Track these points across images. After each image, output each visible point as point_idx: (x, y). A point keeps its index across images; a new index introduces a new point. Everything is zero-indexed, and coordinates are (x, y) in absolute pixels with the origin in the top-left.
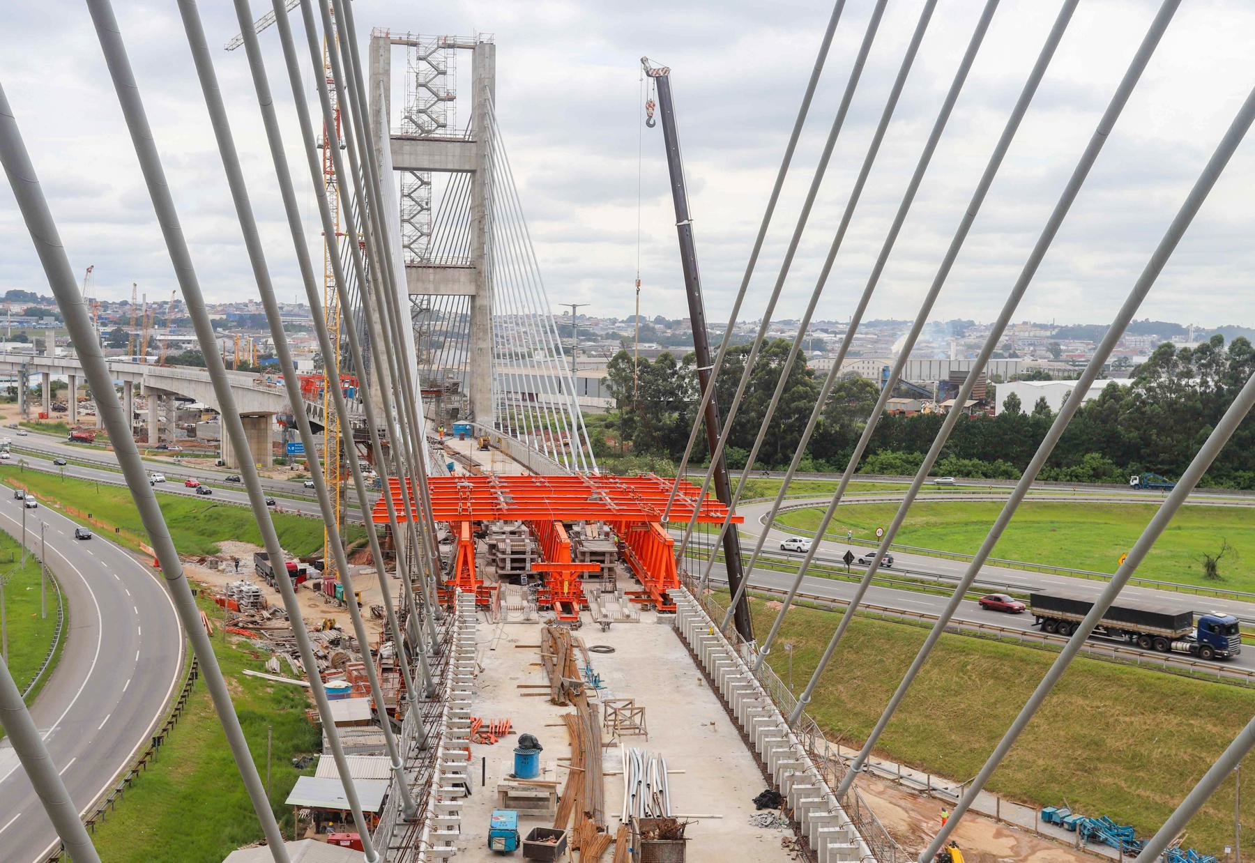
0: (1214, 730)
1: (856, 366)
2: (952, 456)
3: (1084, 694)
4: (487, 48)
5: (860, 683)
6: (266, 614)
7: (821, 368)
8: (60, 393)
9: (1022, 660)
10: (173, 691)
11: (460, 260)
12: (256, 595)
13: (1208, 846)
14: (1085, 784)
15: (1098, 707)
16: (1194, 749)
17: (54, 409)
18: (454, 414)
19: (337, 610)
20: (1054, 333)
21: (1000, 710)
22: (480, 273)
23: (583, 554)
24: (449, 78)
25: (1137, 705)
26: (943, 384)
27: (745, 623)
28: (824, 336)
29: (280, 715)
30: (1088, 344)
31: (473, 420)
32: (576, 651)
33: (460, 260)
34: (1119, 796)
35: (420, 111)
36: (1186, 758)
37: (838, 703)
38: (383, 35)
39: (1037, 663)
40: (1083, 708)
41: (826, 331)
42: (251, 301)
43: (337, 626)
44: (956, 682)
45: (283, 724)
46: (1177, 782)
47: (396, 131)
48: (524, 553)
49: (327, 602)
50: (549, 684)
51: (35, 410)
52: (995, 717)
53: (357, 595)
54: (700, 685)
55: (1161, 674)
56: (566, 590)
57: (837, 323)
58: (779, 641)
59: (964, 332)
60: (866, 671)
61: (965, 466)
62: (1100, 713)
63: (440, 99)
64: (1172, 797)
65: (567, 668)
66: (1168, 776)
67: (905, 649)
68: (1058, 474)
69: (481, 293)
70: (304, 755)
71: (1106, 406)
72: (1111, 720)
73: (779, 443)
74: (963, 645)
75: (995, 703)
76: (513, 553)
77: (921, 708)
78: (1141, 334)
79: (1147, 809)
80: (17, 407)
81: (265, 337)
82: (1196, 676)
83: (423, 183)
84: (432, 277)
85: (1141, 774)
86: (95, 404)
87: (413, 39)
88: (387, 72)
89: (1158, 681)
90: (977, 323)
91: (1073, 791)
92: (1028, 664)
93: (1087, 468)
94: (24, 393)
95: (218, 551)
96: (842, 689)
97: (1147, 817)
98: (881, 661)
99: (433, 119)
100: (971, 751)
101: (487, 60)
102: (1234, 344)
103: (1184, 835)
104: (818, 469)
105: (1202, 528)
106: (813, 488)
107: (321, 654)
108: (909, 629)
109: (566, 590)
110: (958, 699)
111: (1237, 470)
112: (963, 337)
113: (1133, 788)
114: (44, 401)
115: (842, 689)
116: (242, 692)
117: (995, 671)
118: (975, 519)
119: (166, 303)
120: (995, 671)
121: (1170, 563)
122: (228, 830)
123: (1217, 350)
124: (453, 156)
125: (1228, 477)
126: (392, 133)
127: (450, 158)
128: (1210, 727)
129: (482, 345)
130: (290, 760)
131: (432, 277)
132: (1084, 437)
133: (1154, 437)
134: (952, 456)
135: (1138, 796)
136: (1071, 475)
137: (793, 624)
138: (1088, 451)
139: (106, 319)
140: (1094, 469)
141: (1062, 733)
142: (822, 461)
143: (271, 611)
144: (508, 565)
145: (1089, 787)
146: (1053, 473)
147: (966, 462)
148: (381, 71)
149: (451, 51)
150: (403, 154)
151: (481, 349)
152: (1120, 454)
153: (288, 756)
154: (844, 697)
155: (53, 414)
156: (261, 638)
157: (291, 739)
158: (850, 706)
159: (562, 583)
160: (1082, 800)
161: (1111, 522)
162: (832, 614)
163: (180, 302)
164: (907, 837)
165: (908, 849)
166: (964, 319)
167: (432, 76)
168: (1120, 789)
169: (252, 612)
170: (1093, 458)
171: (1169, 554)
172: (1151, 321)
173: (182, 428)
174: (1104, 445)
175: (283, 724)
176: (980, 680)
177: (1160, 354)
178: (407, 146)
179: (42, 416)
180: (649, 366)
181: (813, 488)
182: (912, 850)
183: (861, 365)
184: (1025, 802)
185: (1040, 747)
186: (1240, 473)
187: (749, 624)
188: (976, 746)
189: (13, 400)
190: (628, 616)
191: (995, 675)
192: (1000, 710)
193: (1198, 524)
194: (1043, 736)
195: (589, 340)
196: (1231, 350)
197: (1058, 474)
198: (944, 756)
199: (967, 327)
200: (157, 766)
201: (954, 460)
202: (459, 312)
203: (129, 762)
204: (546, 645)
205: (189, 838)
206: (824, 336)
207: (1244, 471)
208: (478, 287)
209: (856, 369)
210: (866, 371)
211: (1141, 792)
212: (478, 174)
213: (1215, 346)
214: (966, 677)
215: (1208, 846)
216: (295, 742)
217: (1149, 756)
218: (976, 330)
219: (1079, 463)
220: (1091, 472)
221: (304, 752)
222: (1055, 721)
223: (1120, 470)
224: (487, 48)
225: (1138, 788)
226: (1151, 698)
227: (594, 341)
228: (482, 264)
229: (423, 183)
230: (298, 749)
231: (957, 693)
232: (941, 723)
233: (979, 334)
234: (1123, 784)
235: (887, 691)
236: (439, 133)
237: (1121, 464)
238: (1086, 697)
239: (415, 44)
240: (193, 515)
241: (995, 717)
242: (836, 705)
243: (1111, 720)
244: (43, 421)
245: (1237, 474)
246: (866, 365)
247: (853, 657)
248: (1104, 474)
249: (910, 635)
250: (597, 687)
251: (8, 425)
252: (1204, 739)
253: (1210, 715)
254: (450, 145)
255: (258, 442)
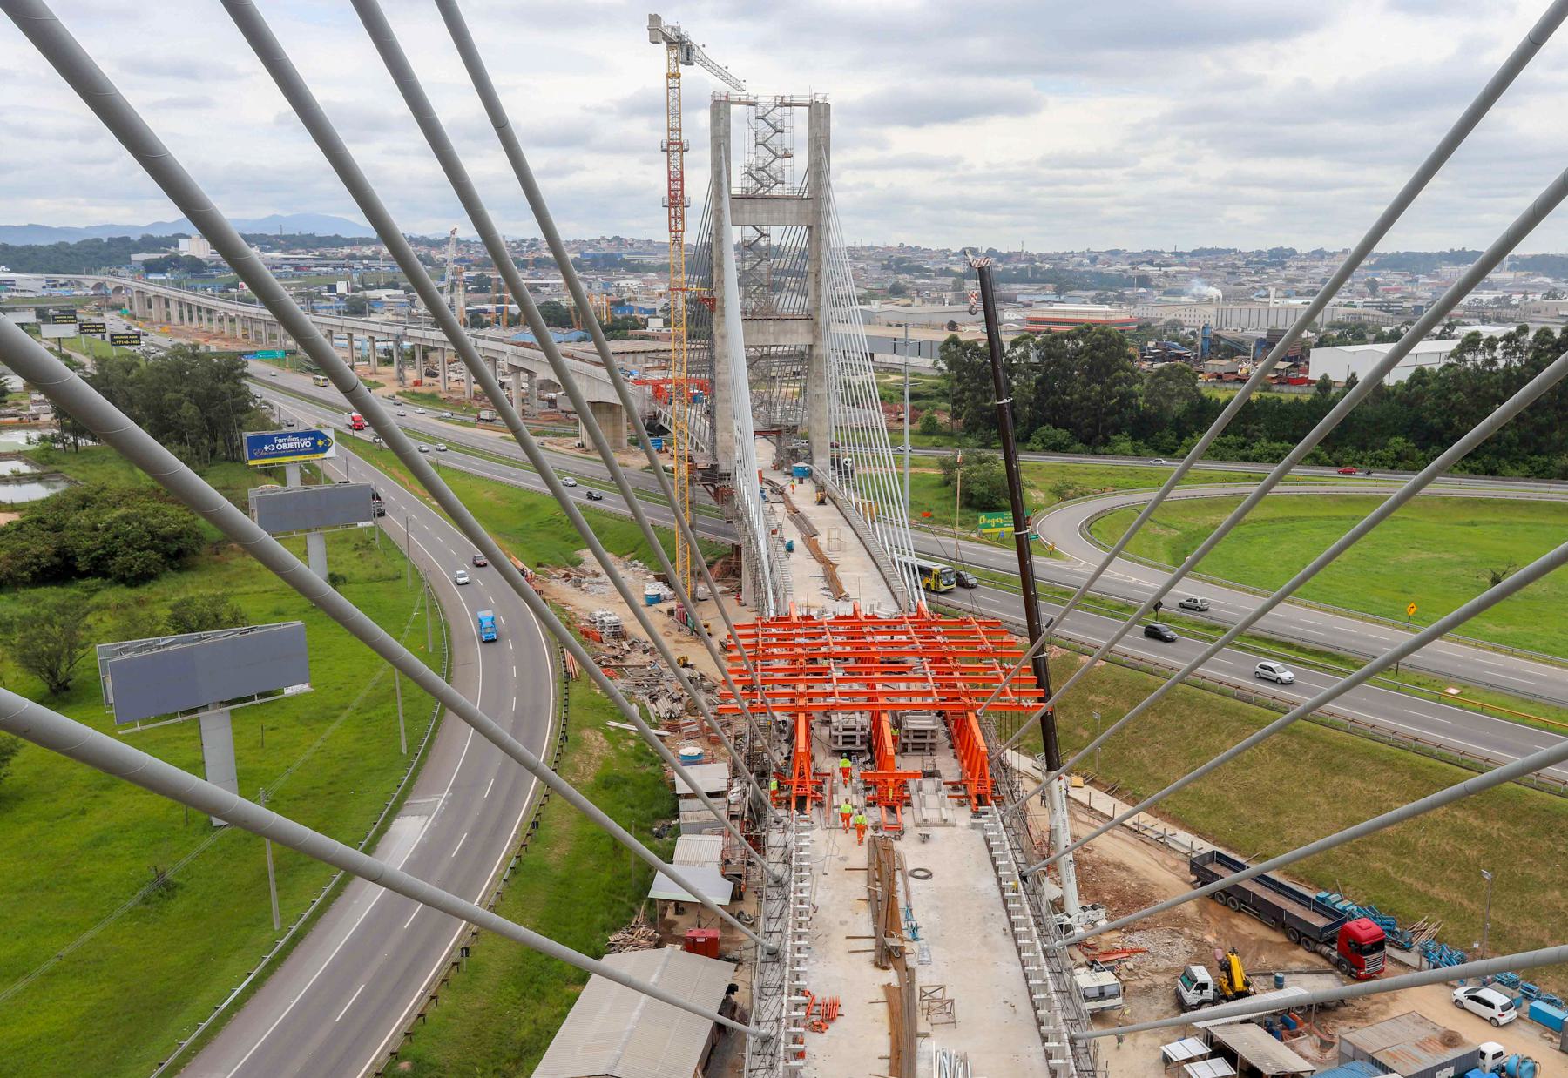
0: (1475, 823)
1: (1178, 313)
2: (1263, 439)
3: (1362, 778)
4: (822, 108)
5: (1161, 747)
6: (625, 645)
7: (1145, 316)
8: (432, 355)
9: (1308, 738)
10: (546, 752)
11: (798, 266)
12: (616, 625)
13: (1459, 937)
14: (1356, 867)
15: (1374, 792)
16: (1456, 841)
17: (427, 374)
18: (794, 454)
19: (688, 639)
20: (1372, 263)
21: (1285, 787)
22: (817, 324)
23: (908, 731)
24: (786, 135)
25: (1409, 792)
26: (1260, 342)
27: (1054, 755)
28: (1150, 270)
29: (641, 775)
30: (1405, 275)
31: (811, 463)
32: (898, 873)
33: (798, 266)
34: (1386, 882)
35: (758, 169)
36: (1448, 848)
37: (1141, 766)
38: (724, 99)
39: (1323, 742)
40: (1360, 791)
41: (1150, 263)
42: (603, 238)
43: (689, 663)
44: (1248, 755)
45: (644, 788)
46: (1438, 872)
47: (736, 191)
48: (854, 729)
49: (680, 630)
50: (873, 935)
51: (411, 374)
52: (1282, 793)
53: (706, 626)
54: (1006, 934)
55: (1432, 762)
56: (890, 796)
57: (1162, 252)
58: (1090, 698)
59: (1285, 263)
60: (1167, 736)
61: (1276, 449)
62: (1375, 797)
63: (777, 157)
64: (1433, 886)
65: (889, 912)
66: (1431, 865)
67: (1204, 717)
68: (1363, 457)
69: (818, 343)
70: (663, 822)
71: (1413, 390)
72: (1385, 805)
73: (1101, 425)
74: (1257, 717)
75: (1282, 780)
76: (844, 730)
77: (1216, 778)
78: (1457, 264)
79: (1409, 896)
80: (392, 370)
81: (616, 280)
82: (1465, 764)
83: (763, 235)
84: (771, 329)
85: (1407, 861)
86: (463, 367)
87: (752, 100)
88: (728, 135)
89: (1429, 770)
90: (1299, 251)
91: (1345, 873)
92: (1313, 742)
93: (1391, 451)
94: (399, 354)
95: (581, 562)
96: (1144, 752)
97: (1409, 904)
98: (1182, 727)
99: (770, 176)
100: (1258, 825)
101: (822, 120)
102: (1538, 334)
103: (1440, 924)
104: (1138, 455)
105: (1494, 523)
106: (1131, 475)
107: (675, 696)
108: (1207, 695)
109: (890, 796)
110: (1249, 772)
111: (1532, 454)
112: (1284, 268)
113: (1399, 874)
114: (417, 365)
115: (1144, 752)
116: (607, 747)
117: (1284, 746)
118: (1280, 514)
119: (524, 241)
120: (1284, 746)
121: (1460, 570)
122: (600, 918)
123: (1521, 338)
124: (791, 213)
125: (1523, 461)
126: (733, 193)
127: (788, 215)
128: (1471, 820)
129: (819, 391)
130: (650, 830)
131: (771, 329)
132: (1390, 422)
133: (1457, 423)
134: (1263, 439)
135: (1403, 882)
136: (1376, 459)
137: (1103, 682)
138: (1394, 434)
139: (470, 261)
140: (1397, 453)
141: (1340, 814)
142: (1141, 443)
143: (630, 642)
144: (840, 742)
145: (1360, 871)
146: (1358, 457)
147: (1277, 445)
148: (722, 133)
149: (787, 109)
150: (743, 213)
151: (818, 396)
152: (1422, 437)
153: (649, 825)
154: (1146, 761)
155: (427, 380)
156: (622, 677)
157: (651, 806)
158: (1151, 770)
159: (887, 791)
160: (1353, 882)
161: (1410, 516)
162: (1139, 673)
163: (536, 240)
164: (1194, 920)
165: (1195, 934)
166: (1286, 247)
167: (770, 160)
168: (1387, 874)
169: (614, 643)
170: (1398, 442)
171: (1459, 559)
172: (1467, 250)
173: (544, 400)
174: (1408, 429)
175: (644, 788)
176: (1270, 754)
177: (1469, 342)
178: (747, 205)
179: (417, 383)
180: (979, 349)
181: (1131, 475)
182: (1198, 936)
183: (1183, 313)
184: (1302, 881)
185: (1319, 827)
186: (1536, 457)
187: (1057, 755)
188: (1262, 821)
189: (389, 362)
190: (946, 820)
191: (1283, 750)
192: (1285, 787)
193: (1489, 519)
194: (1322, 815)
195: (924, 277)
196: (1535, 339)
197: (1363, 457)
198: (1234, 829)
199: (1288, 257)
200: (537, 846)
201: (1265, 443)
202: (799, 245)
203: (512, 842)
204: (872, 868)
205: (567, 929)
206: (1150, 270)
207: (1539, 456)
208: (816, 337)
209: (1178, 317)
210: (1187, 319)
211: (1408, 880)
212: (814, 229)
213: (1521, 334)
214: (1257, 751)
215: (1459, 937)
216: (655, 809)
217: (1415, 845)
218: (1298, 260)
219: (1383, 447)
220: (1395, 456)
221: (663, 818)
222: (1334, 802)
223: (1422, 454)
224: (822, 108)
225: (1403, 874)
226: (1422, 785)
227: (929, 277)
228: (818, 315)
229: (763, 235)
230: (657, 816)
231: (1248, 767)
232: (1232, 795)
233: (1300, 265)
234: (1390, 870)
235: (1185, 758)
236: (777, 191)
237: (1422, 448)
238: (1363, 780)
239: (754, 104)
240: (559, 518)
241: (1282, 793)
242: (1138, 768)
243: (1385, 805)
244: (418, 389)
245: (1532, 458)
246: (1187, 313)
247: (1156, 720)
248: (1407, 458)
249: (1209, 702)
250: (915, 938)
251: (387, 395)
252: (1465, 831)
253: (1473, 808)
254: (787, 202)
255: (614, 425)
